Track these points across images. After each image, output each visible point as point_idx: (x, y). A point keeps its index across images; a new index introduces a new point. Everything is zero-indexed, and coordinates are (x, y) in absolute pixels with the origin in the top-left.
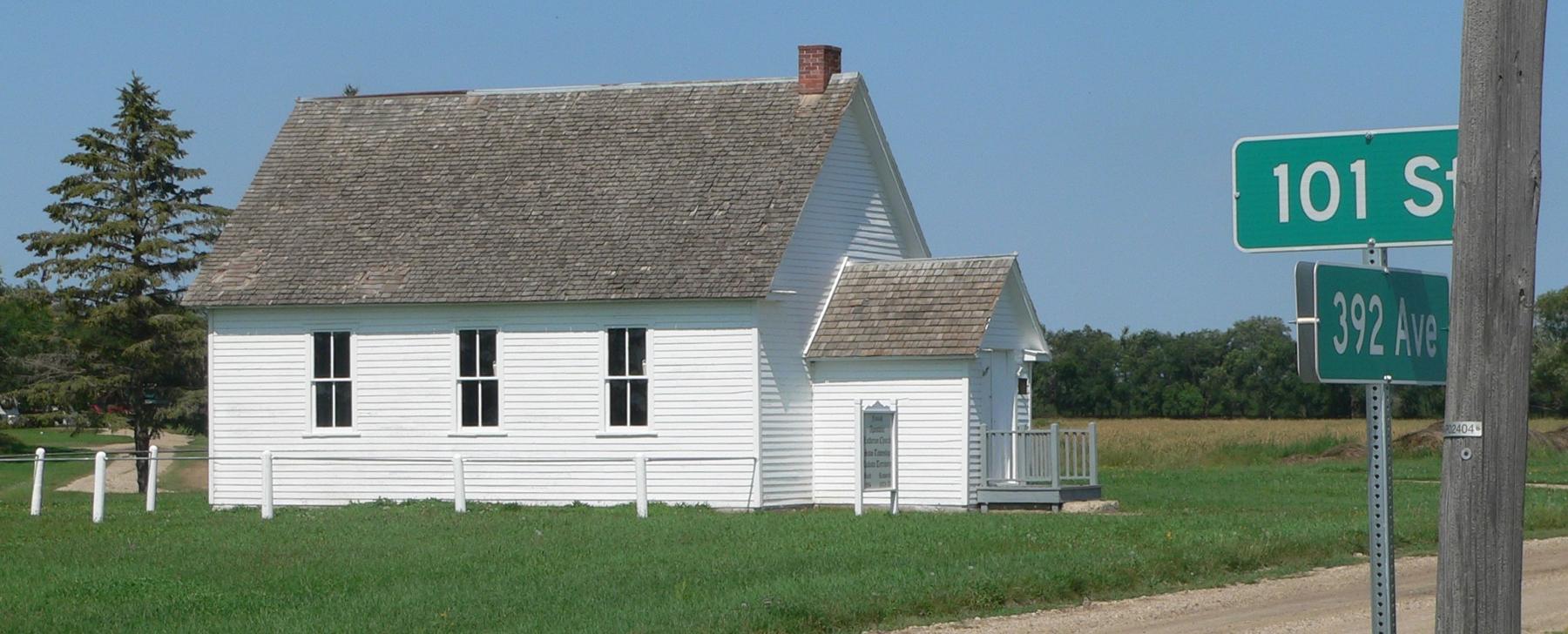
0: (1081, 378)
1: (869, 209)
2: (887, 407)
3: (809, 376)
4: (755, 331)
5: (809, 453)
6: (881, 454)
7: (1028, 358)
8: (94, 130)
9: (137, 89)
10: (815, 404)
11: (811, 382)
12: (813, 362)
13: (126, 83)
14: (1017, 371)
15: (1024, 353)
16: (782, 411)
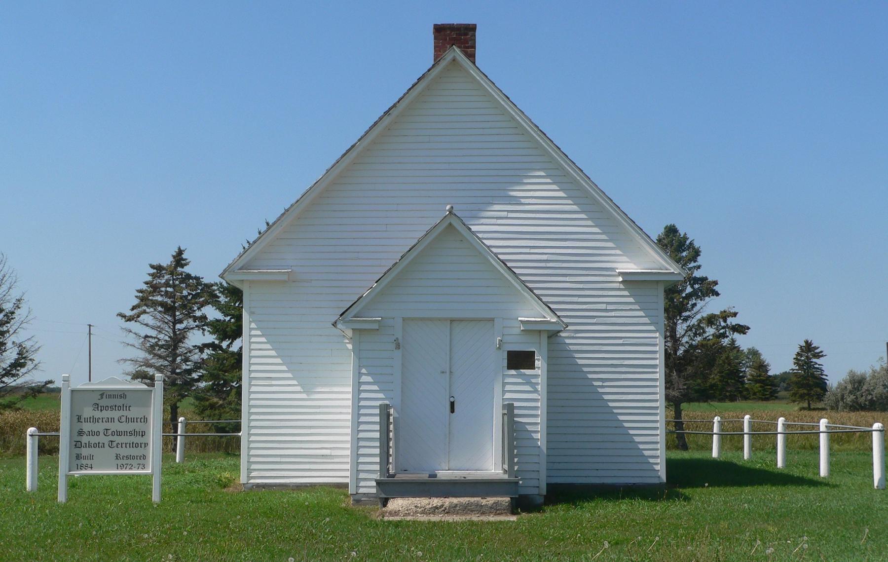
1: (526, 181)
6: (137, 445)
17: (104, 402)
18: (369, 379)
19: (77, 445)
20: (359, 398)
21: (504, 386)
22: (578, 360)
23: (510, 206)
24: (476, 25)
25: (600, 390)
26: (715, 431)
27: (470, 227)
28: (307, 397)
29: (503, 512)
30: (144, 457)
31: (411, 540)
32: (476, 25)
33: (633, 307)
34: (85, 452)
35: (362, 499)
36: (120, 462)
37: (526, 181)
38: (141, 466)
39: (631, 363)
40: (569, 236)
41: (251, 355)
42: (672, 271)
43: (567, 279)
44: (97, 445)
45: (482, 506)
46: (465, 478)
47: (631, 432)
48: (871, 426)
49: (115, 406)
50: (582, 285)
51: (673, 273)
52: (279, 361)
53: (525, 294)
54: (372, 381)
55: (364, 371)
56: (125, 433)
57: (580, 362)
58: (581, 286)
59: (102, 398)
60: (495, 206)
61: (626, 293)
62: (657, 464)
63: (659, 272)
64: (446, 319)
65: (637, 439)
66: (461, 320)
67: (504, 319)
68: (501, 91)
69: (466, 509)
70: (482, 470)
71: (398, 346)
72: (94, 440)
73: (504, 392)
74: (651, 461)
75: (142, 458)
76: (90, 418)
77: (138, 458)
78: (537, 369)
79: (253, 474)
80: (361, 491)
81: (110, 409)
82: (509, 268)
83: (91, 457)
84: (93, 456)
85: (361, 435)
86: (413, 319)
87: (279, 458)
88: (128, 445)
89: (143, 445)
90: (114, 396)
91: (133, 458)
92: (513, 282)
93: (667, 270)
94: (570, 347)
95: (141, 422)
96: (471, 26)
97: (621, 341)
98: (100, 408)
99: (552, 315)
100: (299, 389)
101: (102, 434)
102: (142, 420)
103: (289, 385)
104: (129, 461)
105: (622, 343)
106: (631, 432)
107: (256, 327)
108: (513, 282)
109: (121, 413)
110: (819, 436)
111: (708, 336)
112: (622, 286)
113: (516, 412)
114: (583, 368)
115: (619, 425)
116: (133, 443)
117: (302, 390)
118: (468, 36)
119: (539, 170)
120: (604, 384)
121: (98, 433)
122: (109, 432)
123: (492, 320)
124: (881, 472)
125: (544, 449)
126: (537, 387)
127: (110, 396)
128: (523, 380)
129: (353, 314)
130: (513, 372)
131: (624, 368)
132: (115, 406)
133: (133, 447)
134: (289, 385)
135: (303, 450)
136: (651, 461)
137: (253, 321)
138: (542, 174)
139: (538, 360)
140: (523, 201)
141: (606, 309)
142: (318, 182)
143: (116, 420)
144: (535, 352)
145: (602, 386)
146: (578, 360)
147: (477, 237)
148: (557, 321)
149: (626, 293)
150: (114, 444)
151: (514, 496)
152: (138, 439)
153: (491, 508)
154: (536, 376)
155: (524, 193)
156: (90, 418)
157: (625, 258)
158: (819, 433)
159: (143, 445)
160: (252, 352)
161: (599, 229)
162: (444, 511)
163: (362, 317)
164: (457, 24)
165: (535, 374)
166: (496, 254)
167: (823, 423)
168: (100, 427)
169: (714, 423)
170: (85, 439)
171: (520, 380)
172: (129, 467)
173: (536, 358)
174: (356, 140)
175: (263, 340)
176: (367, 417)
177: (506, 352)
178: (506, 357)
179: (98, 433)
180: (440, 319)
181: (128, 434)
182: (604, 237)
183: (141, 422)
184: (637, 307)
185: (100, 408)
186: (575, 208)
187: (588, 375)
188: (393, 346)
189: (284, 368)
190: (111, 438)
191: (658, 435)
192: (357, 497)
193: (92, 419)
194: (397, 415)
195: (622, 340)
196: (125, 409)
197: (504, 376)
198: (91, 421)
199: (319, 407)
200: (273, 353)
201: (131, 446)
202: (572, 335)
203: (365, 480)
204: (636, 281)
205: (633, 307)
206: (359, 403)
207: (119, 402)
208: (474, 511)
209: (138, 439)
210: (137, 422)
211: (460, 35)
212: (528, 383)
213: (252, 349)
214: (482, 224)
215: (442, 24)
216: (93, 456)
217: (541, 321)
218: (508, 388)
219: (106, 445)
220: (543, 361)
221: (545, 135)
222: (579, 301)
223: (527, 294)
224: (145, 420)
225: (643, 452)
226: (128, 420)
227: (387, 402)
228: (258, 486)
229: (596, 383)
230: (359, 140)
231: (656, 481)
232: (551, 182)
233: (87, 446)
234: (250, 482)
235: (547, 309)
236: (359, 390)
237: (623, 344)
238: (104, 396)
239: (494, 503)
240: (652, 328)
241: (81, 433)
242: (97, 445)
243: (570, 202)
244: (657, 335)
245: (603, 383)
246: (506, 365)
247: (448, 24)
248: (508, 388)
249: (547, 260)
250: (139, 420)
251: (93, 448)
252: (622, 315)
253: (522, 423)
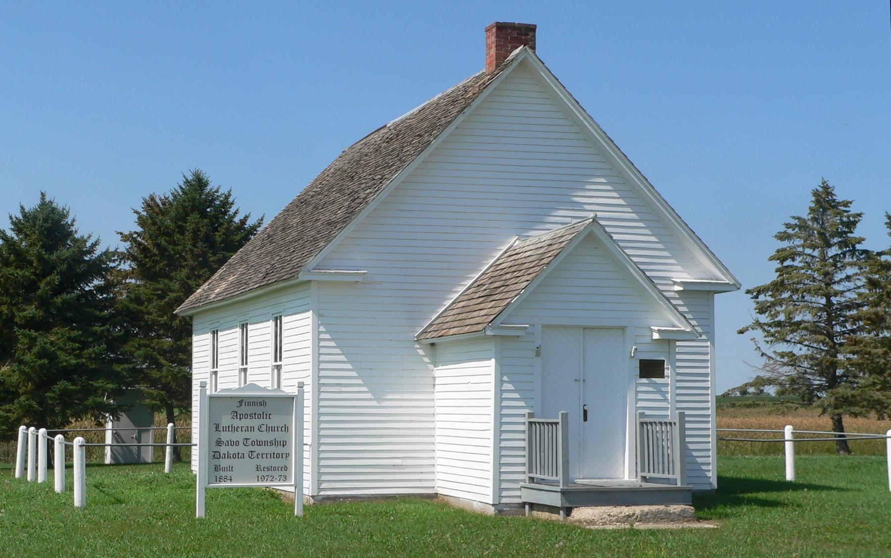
0: (57, 342)
1: (588, 187)
2: (265, 389)
3: (426, 360)
4: (310, 314)
5: (431, 447)
6: (278, 456)
7: (656, 336)
8: (793, 217)
9: (826, 188)
10: (437, 396)
11: (431, 366)
12: (433, 344)
13: (817, 185)
14: (631, 352)
15: (652, 331)
16: (687, 412)
17: (244, 410)
18: (510, 387)
19: (216, 455)
21: (636, 395)
23: (573, 212)
24: (536, 25)
26: (786, 438)
27: (612, 235)
28: (377, 405)
29: (691, 519)
30: (286, 468)
31: (849, 540)
32: (536, 25)
34: (224, 463)
35: (505, 509)
36: (261, 473)
37: (588, 187)
38: (282, 478)
39: (686, 372)
41: (320, 360)
42: (727, 282)
44: (235, 456)
45: (670, 514)
46: (641, 486)
48: (885, 433)
49: (255, 414)
51: (729, 283)
52: (349, 366)
54: (514, 389)
55: (505, 378)
56: (265, 443)
59: (241, 405)
62: (709, 471)
63: (716, 283)
64: (579, 327)
66: (593, 328)
67: (636, 328)
68: (571, 95)
69: (656, 517)
70: (614, 479)
71: (538, 354)
72: (233, 450)
75: (283, 469)
76: (229, 427)
77: (280, 469)
78: (666, 378)
79: (323, 486)
80: (504, 501)
81: (249, 417)
82: (648, 277)
83: (231, 469)
84: (232, 467)
85: (503, 444)
87: (350, 469)
88: (269, 456)
89: (284, 456)
90: (254, 404)
91: (275, 469)
92: (650, 291)
93: (717, 280)
95: (282, 431)
96: (531, 26)
98: (238, 416)
99: (687, 325)
100: (369, 396)
101: (241, 443)
102: (283, 429)
103: (360, 392)
104: (270, 473)
107: (325, 330)
108: (650, 291)
109: (261, 421)
110: (784, 444)
111: (851, 345)
112: (677, 296)
116: (274, 454)
117: (373, 398)
121: (237, 443)
122: (249, 442)
123: (623, 329)
126: (666, 395)
127: (249, 404)
128: (654, 389)
130: (645, 380)
132: (255, 414)
133: (274, 458)
134: (360, 392)
135: (374, 460)
136: (704, 468)
137: (322, 324)
139: (668, 369)
140: (586, 207)
143: (256, 429)
144: (664, 361)
147: (618, 245)
148: (692, 331)
150: (255, 454)
152: (279, 450)
153: (679, 515)
154: (666, 385)
155: (587, 199)
156: (229, 427)
157: (679, 268)
158: (104, 446)
159: (284, 456)
160: (321, 356)
161: (656, 237)
162: (636, 519)
164: (518, 24)
165: (665, 382)
166: (635, 263)
167: (788, 431)
168: (239, 436)
169: (167, 430)
170: (223, 449)
171: (651, 389)
172: (270, 478)
173: (665, 366)
175: (333, 344)
176: (509, 426)
177: (639, 361)
178: (639, 366)
179: (237, 443)
180: (573, 327)
181: (269, 444)
182: (660, 246)
183: (282, 431)
185: (238, 416)
186: (634, 216)
188: (534, 354)
189: (354, 374)
190: (251, 448)
191: (709, 442)
192: (499, 507)
193: (230, 428)
196: (265, 417)
197: (637, 384)
198: (230, 430)
199: (390, 415)
200: (343, 358)
201: (272, 456)
203: (507, 489)
204: (698, 291)
206: (501, 411)
207: (259, 410)
208: (664, 519)
209: (279, 450)
210: (278, 431)
211: (521, 34)
212: (659, 392)
213: (321, 354)
216: (232, 467)
217: (677, 330)
219: (246, 456)
221: (613, 142)
223: (662, 303)
224: (286, 429)
225: (697, 459)
226: (270, 429)
228: (328, 498)
231: (708, 488)
232: (612, 189)
233: (226, 457)
234: (320, 494)
235: (682, 318)
238: (243, 404)
239: (682, 511)
241: (219, 443)
242: (235, 456)
248: (640, 396)
250: (280, 429)
251: (232, 459)
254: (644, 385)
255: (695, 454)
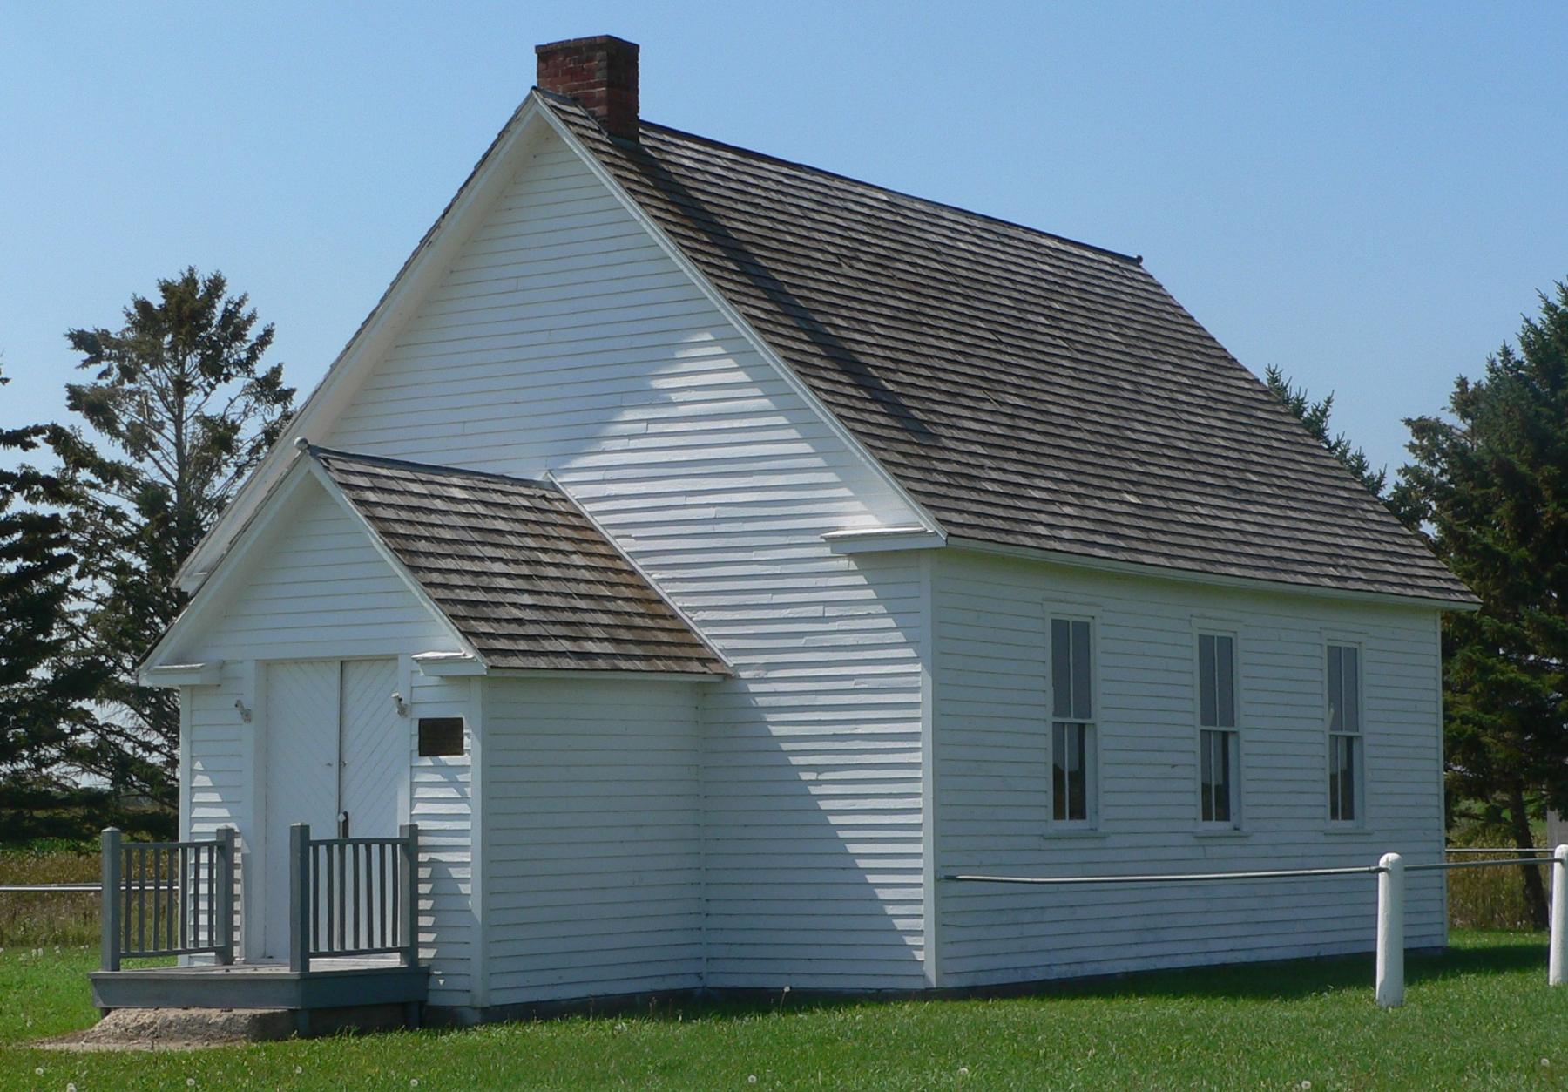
1: (679, 355)
20: (191, 818)
21: (412, 791)
22: (772, 728)
25: (814, 790)
33: (872, 609)
37: (679, 355)
40: (755, 464)
43: (752, 556)
45: (209, 1025)
47: (872, 879)
50: (779, 567)
53: (425, 605)
57: (776, 731)
58: (777, 569)
60: (626, 412)
61: (860, 580)
62: (919, 948)
65: (884, 894)
73: (413, 801)
74: (909, 940)
78: (466, 755)
86: (282, 662)
94: (757, 699)
96: (598, 41)
97: (850, 685)
105: (852, 687)
106: (872, 879)
113: (422, 840)
114: (781, 745)
115: (847, 864)
118: (593, 64)
119: (703, 328)
120: (820, 778)
123: (392, 658)
124: (1386, 967)
125: (478, 913)
129: (160, 660)
130: (428, 761)
131: (858, 742)
136: (909, 940)
138: (708, 337)
140: (675, 397)
141: (824, 617)
142: (319, 393)
144: (461, 719)
145: (817, 780)
146: (772, 728)
149: (861, 580)
151: (294, 1008)
153: (222, 1028)
154: (463, 769)
157: (857, 506)
162: (153, 1033)
163: (187, 663)
165: (463, 763)
171: (438, 778)
173: (465, 731)
174: (377, 303)
177: (416, 725)
182: (818, 462)
184: (881, 609)
186: (765, 403)
187: (790, 758)
188: (236, 716)
194: (246, 850)
195: (853, 682)
202: (762, 674)
205: (872, 609)
212: (452, 783)
214: (604, 452)
215: (549, 44)
217: (446, 658)
218: (421, 793)
220: (475, 738)
222: (773, 602)
227: (232, 825)
229: (805, 776)
230: (382, 301)
236: (191, 803)
237: (854, 689)
240: (909, 653)
243: (757, 392)
244: (918, 668)
245: (819, 774)
246: (416, 747)
247: (559, 43)
249: (715, 518)
252: (852, 628)
253: (441, 862)
254: (427, 769)
255: (890, 910)
